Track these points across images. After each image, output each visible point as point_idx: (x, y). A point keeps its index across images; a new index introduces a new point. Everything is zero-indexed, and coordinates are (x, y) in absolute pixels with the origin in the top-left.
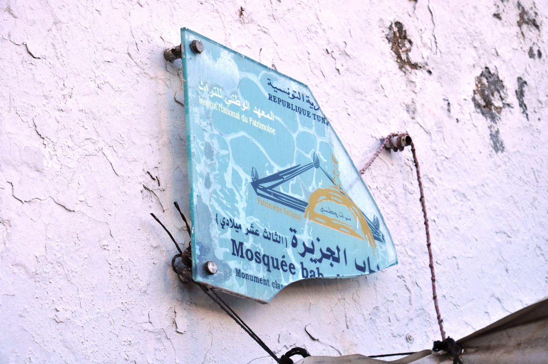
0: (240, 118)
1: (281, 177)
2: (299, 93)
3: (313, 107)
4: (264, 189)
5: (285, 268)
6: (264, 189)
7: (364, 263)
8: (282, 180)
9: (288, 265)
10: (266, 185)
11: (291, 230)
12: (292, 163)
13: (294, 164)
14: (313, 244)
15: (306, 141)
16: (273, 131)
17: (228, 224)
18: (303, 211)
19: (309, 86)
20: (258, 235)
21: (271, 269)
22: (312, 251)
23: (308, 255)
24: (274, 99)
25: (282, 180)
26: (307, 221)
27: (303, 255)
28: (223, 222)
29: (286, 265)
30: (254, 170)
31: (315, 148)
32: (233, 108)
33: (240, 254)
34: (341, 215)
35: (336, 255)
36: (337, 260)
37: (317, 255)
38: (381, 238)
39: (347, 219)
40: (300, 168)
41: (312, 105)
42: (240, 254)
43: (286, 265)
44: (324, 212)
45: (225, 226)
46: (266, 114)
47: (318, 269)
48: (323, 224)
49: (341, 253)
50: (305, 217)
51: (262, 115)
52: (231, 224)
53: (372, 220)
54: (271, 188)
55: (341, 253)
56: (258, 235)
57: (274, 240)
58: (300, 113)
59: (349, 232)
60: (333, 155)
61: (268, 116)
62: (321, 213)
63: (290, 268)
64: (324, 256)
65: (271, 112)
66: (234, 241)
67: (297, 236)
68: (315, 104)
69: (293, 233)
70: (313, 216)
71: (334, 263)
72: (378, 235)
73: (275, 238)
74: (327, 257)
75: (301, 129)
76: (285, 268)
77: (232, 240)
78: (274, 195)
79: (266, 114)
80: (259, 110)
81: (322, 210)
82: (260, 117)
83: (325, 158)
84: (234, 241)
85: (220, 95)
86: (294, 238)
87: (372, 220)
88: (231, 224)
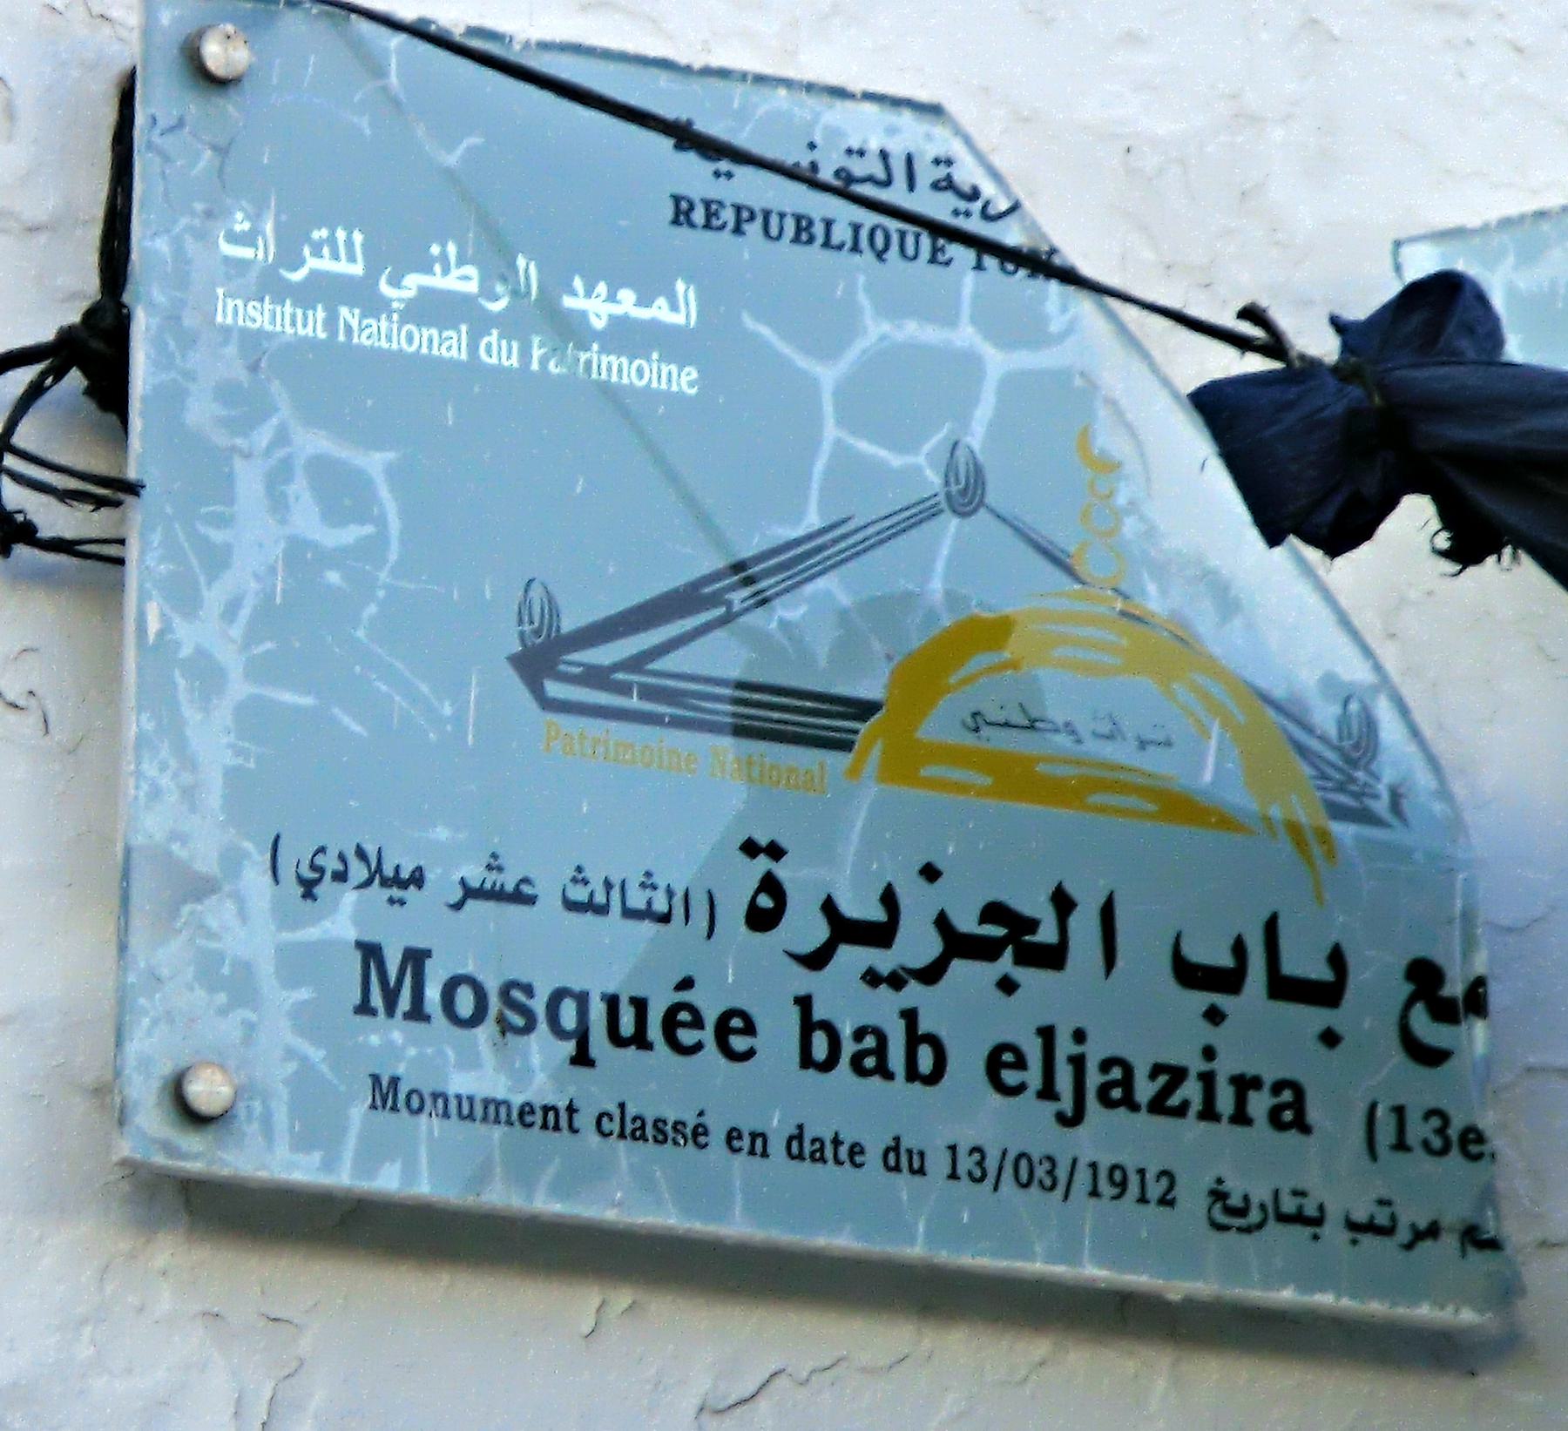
0: (473, 348)
1: (714, 600)
2: (884, 155)
3: (977, 206)
4: (595, 677)
5: (687, 1037)
6: (595, 677)
7: (1239, 949)
8: (722, 610)
9: (710, 1019)
10: (604, 655)
11: (750, 848)
12: (800, 515)
13: (813, 520)
14: (889, 899)
15: (884, 395)
16: (685, 380)
17: (341, 877)
18: (845, 746)
19: (952, 107)
20: (531, 900)
21: (901, 1024)
22: (880, 934)
23: (853, 958)
24: (710, 215)
25: (722, 610)
26: (870, 791)
27: (816, 960)
28: (313, 867)
29: (697, 1023)
30: (536, 593)
31: (964, 421)
32: (433, 309)
33: (404, 1003)
34: (1105, 728)
35: (1047, 934)
36: (1053, 957)
37: (916, 943)
38: (1381, 806)
39: (1143, 744)
40: (835, 541)
41: (974, 195)
42: (404, 1003)
43: (697, 1023)
44: (986, 731)
45: (325, 888)
46: (644, 301)
47: (910, 1016)
48: (983, 793)
49: (1084, 926)
50: (854, 772)
51: (617, 310)
52: (358, 872)
53: (1332, 731)
54: (636, 663)
55: (1084, 926)
56: (531, 900)
57: (629, 913)
58: (880, 255)
59: (1151, 807)
60: (1086, 429)
61: (660, 311)
62: (969, 740)
63: (723, 1031)
64: (957, 945)
65: (680, 286)
66: (371, 952)
67: (782, 871)
68: (988, 189)
69: (763, 863)
70: (904, 765)
71: (1026, 976)
72: (1357, 796)
73: (637, 900)
74: (985, 950)
75: (876, 329)
76: (687, 1037)
77: (360, 945)
78: (648, 693)
79: (644, 301)
80: (602, 288)
81: (977, 722)
82: (599, 324)
83: (175, 685)
84: (371, 952)
85: (352, 258)
86: (770, 884)
87: (1332, 731)
88: (358, 872)
